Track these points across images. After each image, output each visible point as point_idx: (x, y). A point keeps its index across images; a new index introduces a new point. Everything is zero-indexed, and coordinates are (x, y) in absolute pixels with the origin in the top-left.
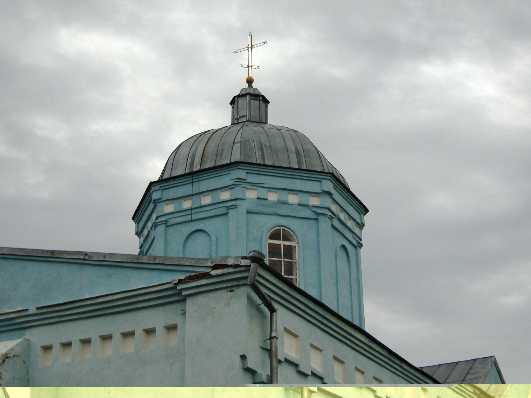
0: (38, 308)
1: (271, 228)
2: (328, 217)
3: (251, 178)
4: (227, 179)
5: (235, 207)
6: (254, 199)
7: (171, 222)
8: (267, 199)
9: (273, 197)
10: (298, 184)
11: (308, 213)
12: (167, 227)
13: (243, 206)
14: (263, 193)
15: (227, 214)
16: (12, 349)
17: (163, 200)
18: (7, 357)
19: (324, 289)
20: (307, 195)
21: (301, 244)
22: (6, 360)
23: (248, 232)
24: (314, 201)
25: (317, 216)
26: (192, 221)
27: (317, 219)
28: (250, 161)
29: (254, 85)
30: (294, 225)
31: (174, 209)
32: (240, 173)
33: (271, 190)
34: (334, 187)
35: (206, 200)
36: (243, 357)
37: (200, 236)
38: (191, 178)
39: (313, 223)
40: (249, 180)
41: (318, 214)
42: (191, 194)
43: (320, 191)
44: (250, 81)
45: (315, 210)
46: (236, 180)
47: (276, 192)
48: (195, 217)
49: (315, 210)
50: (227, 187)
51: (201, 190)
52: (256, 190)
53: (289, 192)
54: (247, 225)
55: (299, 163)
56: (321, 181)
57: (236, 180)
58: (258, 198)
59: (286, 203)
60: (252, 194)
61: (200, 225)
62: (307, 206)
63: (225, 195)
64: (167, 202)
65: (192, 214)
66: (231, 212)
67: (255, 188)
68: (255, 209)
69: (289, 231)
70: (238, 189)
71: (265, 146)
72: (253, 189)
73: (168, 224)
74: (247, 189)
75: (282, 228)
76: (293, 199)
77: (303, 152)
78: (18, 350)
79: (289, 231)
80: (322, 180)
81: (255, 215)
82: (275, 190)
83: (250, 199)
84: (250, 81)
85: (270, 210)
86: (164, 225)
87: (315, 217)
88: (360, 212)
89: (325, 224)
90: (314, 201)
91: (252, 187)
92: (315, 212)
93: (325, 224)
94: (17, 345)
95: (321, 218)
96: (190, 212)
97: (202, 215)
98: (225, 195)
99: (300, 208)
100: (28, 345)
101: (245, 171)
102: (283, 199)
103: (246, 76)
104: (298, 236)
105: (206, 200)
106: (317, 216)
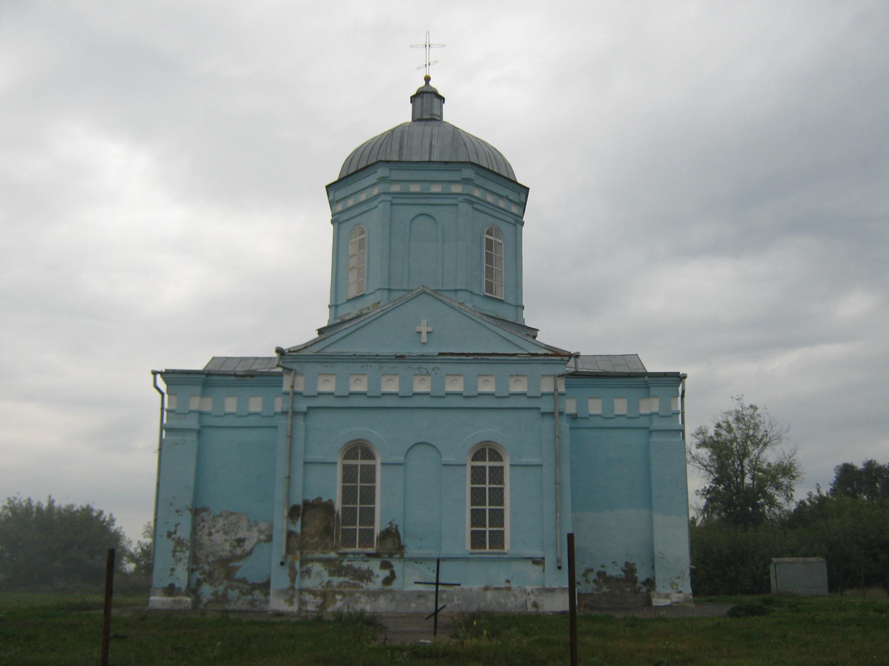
7: (341, 220)
29: (431, 83)
44: (427, 79)
84: (427, 79)
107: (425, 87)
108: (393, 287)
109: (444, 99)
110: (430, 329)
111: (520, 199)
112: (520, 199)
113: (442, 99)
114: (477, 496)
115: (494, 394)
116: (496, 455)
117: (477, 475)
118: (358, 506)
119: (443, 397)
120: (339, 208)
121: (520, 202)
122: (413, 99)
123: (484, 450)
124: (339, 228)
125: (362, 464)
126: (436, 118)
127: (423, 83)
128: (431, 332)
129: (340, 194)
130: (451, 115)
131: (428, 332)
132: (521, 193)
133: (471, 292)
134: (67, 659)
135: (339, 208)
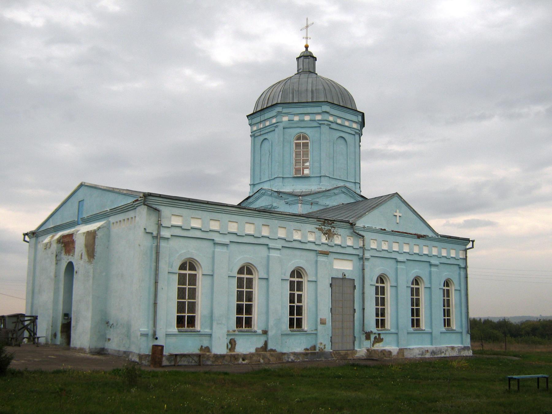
0: (110, 210)
1: (296, 134)
2: (326, 125)
3: (285, 111)
4: (273, 113)
5: (277, 127)
6: (287, 121)
7: (256, 135)
8: (293, 120)
9: (296, 118)
10: (309, 110)
11: (315, 124)
12: (255, 137)
13: (281, 125)
14: (291, 117)
15: (275, 130)
16: (102, 225)
17: (252, 124)
18: (100, 228)
19: (322, 163)
20: (314, 115)
21: (311, 141)
22: (100, 229)
23: (284, 138)
24: (318, 117)
25: (320, 124)
26: (260, 135)
27: (320, 127)
28: (286, 102)
29: (309, 49)
30: (309, 132)
31: (257, 128)
32: (279, 109)
33: (295, 115)
34: (330, 108)
35: (267, 123)
36: (145, 229)
37: (266, 142)
38: (260, 113)
39: (318, 129)
40: (284, 112)
41: (320, 124)
42: (260, 121)
43: (321, 112)
44: (307, 47)
45: (319, 122)
46: (277, 113)
47: (298, 116)
48: (261, 133)
49: (319, 122)
50: (274, 116)
51: (265, 119)
52: (288, 116)
53: (305, 114)
54: (284, 135)
55: (312, 98)
56: (321, 106)
57: (277, 113)
58: (289, 120)
59: (303, 121)
60: (285, 119)
61: (266, 136)
62: (315, 120)
63: (274, 121)
64: (254, 125)
65: (260, 132)
66: (276, 129)
67: (287, 115)
68: (288, 126)
69: (305, 135)
70: (278, 117)
71: (295, 90)
72: (286, 116)
73: (255, 136)
74: (283, 116)
75: (301, 134)
76: (307, 118)
77: (315, 90)
78: (105, 225)
79: (305, 135)
80: (322, 106)
81: (288, 129)
82: (297, 115)
83: (285, 121)
84: (307, 47)
85: (295, 125)
86: (253, 137)
87: (319, 126)
88: (357, 115)
89: (325, 129)
90: (318, 117)
91: (285, 115)
92: (319, 123)
93: (325, 129)
94: (104, 223)
95: (322, 126)
96: (259, 131)
97: (267, 131)
98: (274, 121)
99: (311, 122)
100: (109, 222)
101: (281, 108)
102: (301, 119)
103: (305, 44)
104: (310, 137)
105: (267, 123)
106: (320, 124)
107: (305, 53)
108: (285, 176)
109: (316, 58)
110: (401, 215)
111: (358, 119)
112: (358, 119)
113: (315, 59)
114: (181, 293)
115: (181, 227)
116: (192, 268)
117: (182, 279)
118: (245, 303)
119: (169, 227)
120: (255, 128)
121: (358, 121)
122: (297, 59)
123: (244, 267)
124: (254, 139)
125: (189, 273)
126: (312, 71)
127: (304, 49)
128: (400, 216)
129: (257, 120)
130: (321, 69)
131: (399, 216)
132: (359, 116)
133: (329, 177)
134: (89, 371)
135: (255, 128)
